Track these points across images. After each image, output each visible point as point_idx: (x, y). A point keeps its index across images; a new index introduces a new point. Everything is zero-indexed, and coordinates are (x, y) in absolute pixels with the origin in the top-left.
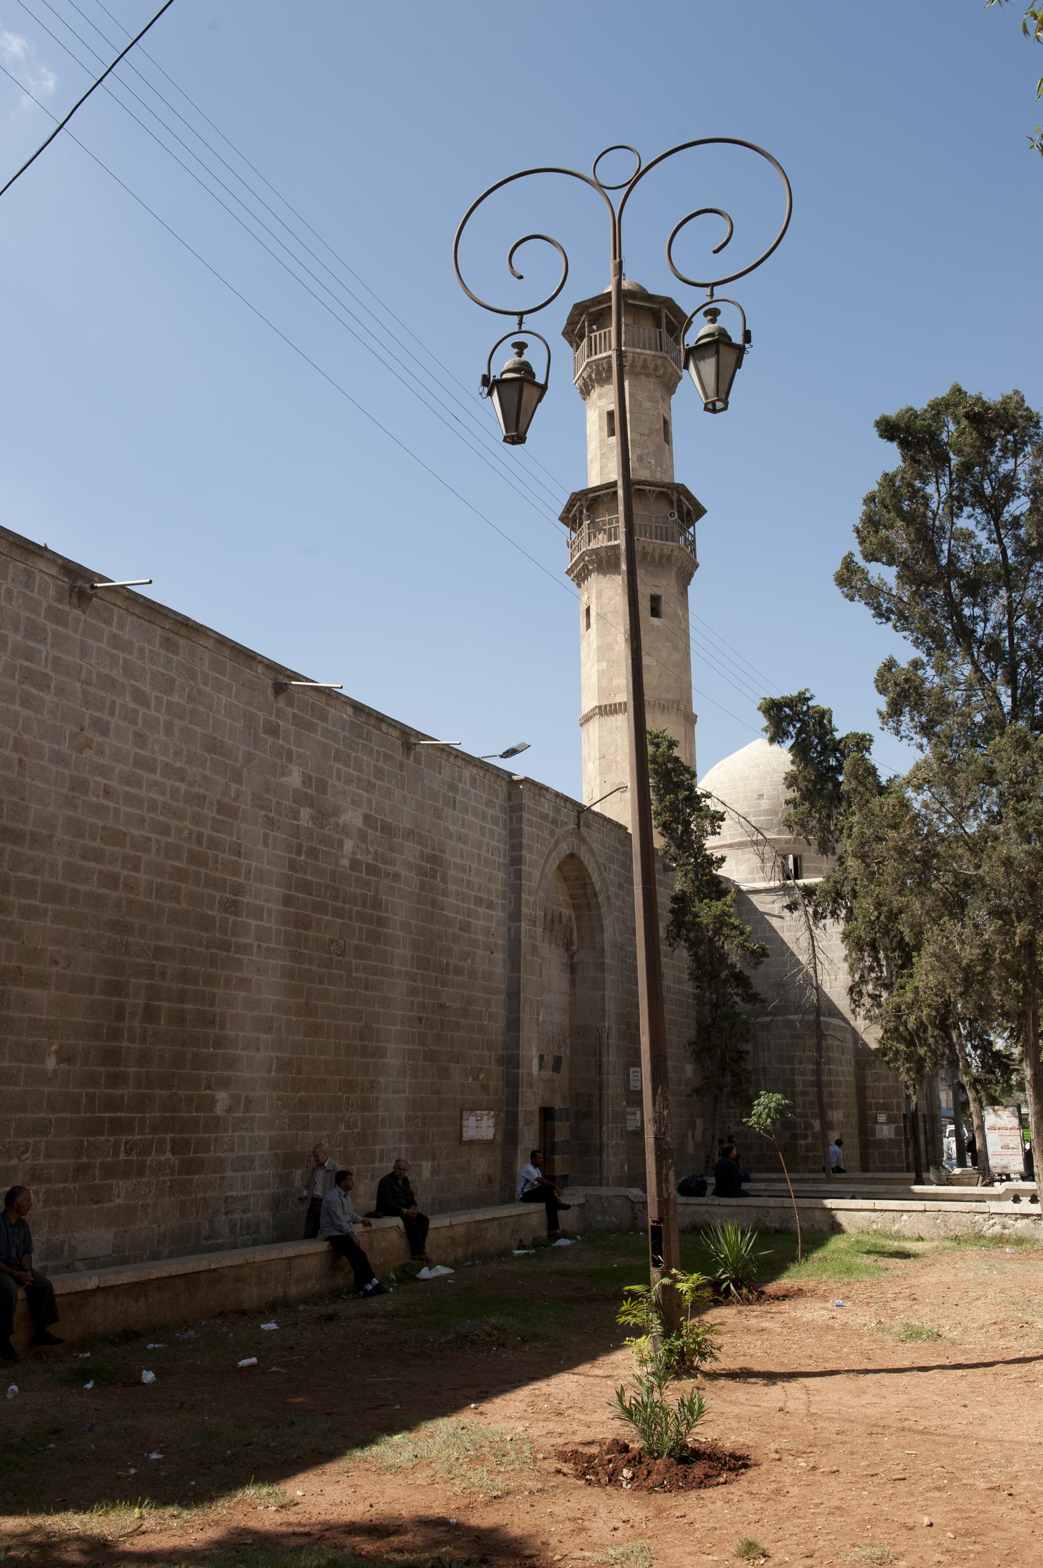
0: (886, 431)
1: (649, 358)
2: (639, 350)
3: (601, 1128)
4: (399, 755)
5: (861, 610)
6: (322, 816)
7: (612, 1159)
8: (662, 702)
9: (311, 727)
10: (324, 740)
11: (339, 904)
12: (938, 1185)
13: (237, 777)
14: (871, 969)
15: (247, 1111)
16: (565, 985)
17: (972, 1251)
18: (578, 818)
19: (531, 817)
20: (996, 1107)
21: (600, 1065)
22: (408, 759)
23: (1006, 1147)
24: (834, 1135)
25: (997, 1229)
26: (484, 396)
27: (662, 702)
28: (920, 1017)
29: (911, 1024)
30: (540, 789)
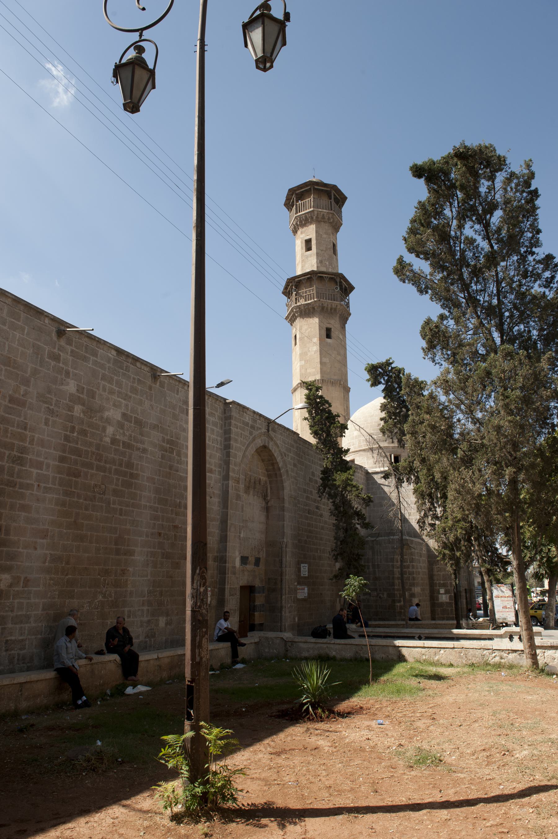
0: (416, 171)
1: (325, 214)
2: (320, 210)
3: (281, 597)
4: (149, 381)
5: (410, 289)
6: (90, 411)
7: (288, 614)
8: (332, 380)
9: (85, 359)
10: (94, 367)
11: (102, 464)
12: (467, 629)
13: (26, 382)
14: (430, 509)
15: (26, 587)
16: (263, 519)
17: (480, 674)
18: (268, 426)
19: (236, 423)
20: (500, 585)
21: (282, 562)
22: (156, 384)
23: (505, 607)
24: (416, 601)
25: (497, 659)
26: (115, 83)
27: (332, 380)
28: (456, 535)
29: (452, 538)
30: (244, 408)
